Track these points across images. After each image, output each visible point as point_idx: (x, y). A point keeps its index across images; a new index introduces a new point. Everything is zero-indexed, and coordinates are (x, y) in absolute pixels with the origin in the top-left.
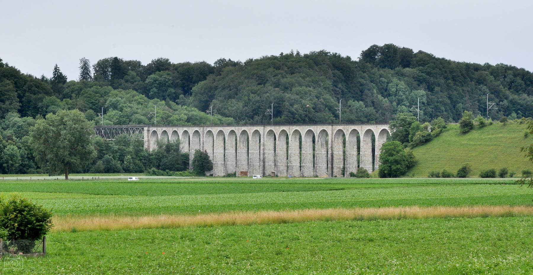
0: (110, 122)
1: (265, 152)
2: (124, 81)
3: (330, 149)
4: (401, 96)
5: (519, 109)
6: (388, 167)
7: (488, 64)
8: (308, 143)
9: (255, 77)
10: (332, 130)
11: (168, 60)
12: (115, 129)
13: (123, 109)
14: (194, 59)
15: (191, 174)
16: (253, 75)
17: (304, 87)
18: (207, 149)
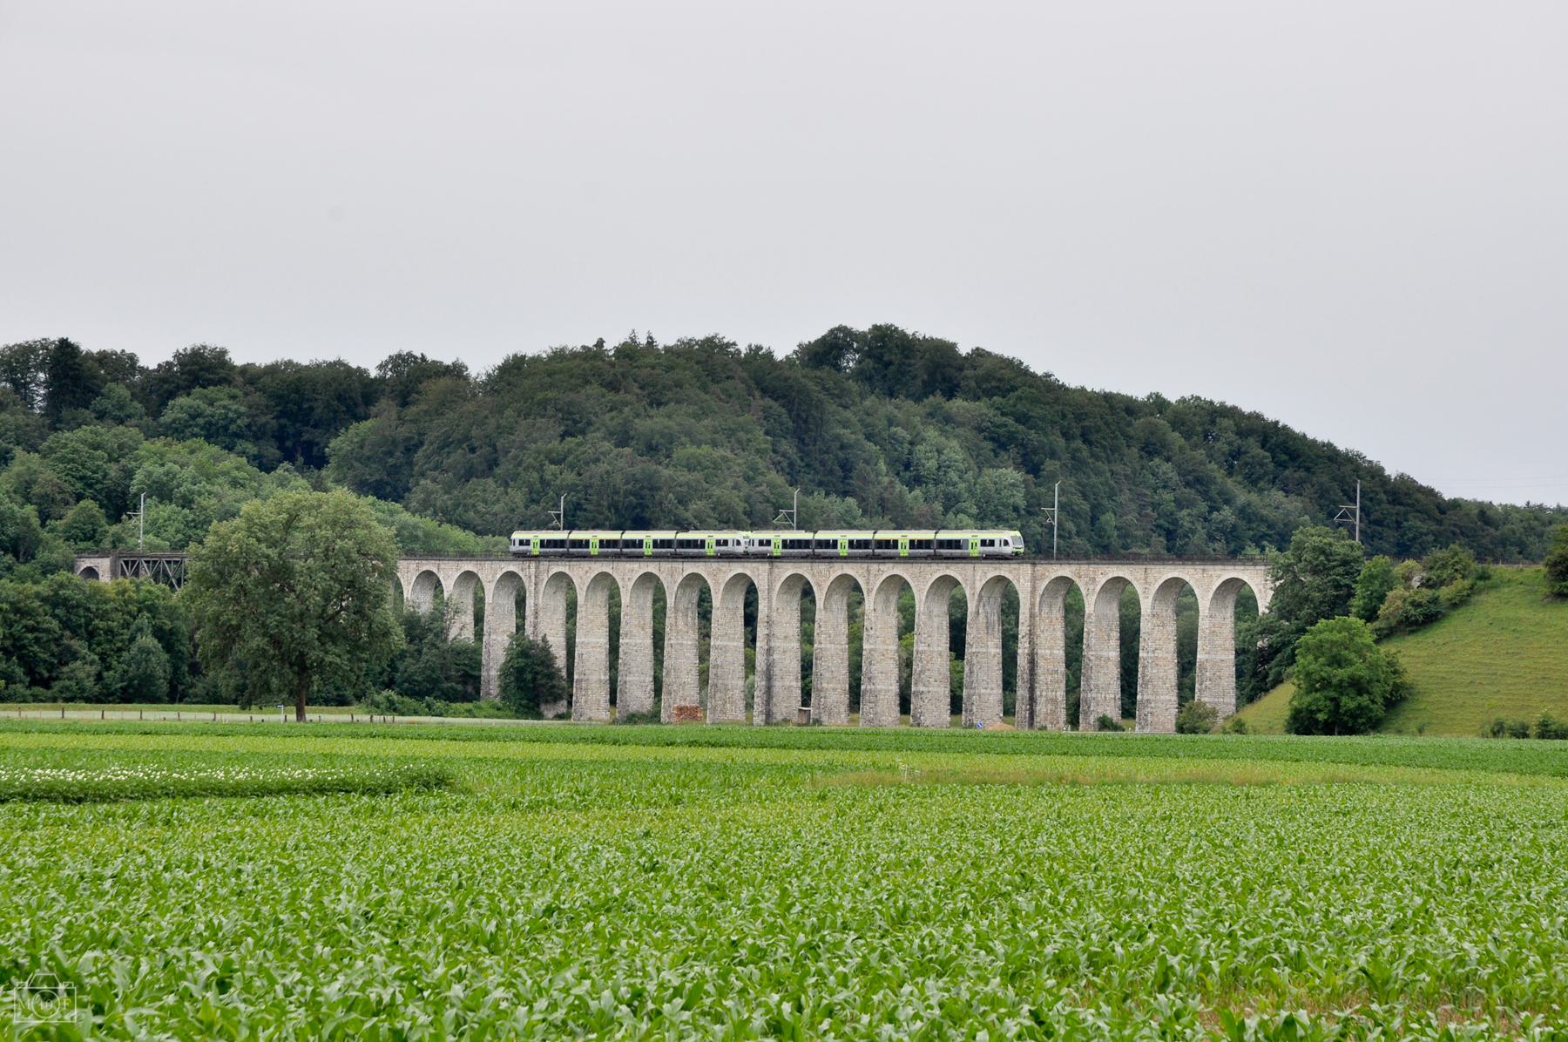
0: (158, 541)
1: (773, 644)
2: (93, 415)
3: (1026, 639)
4: (954, 485)
5: (1264, 536)
6: (1328, 703)
7: (1158, 396)
8: (936, 619)
9: (550, 411)
10: (1034, 580)
11: (223, 353)
12: (176, 562)
13: (192, 501)
14: (308, 351)
15: (500, 713)
16: (543, 404)
17: (706, 449)
18: (547, 631)
